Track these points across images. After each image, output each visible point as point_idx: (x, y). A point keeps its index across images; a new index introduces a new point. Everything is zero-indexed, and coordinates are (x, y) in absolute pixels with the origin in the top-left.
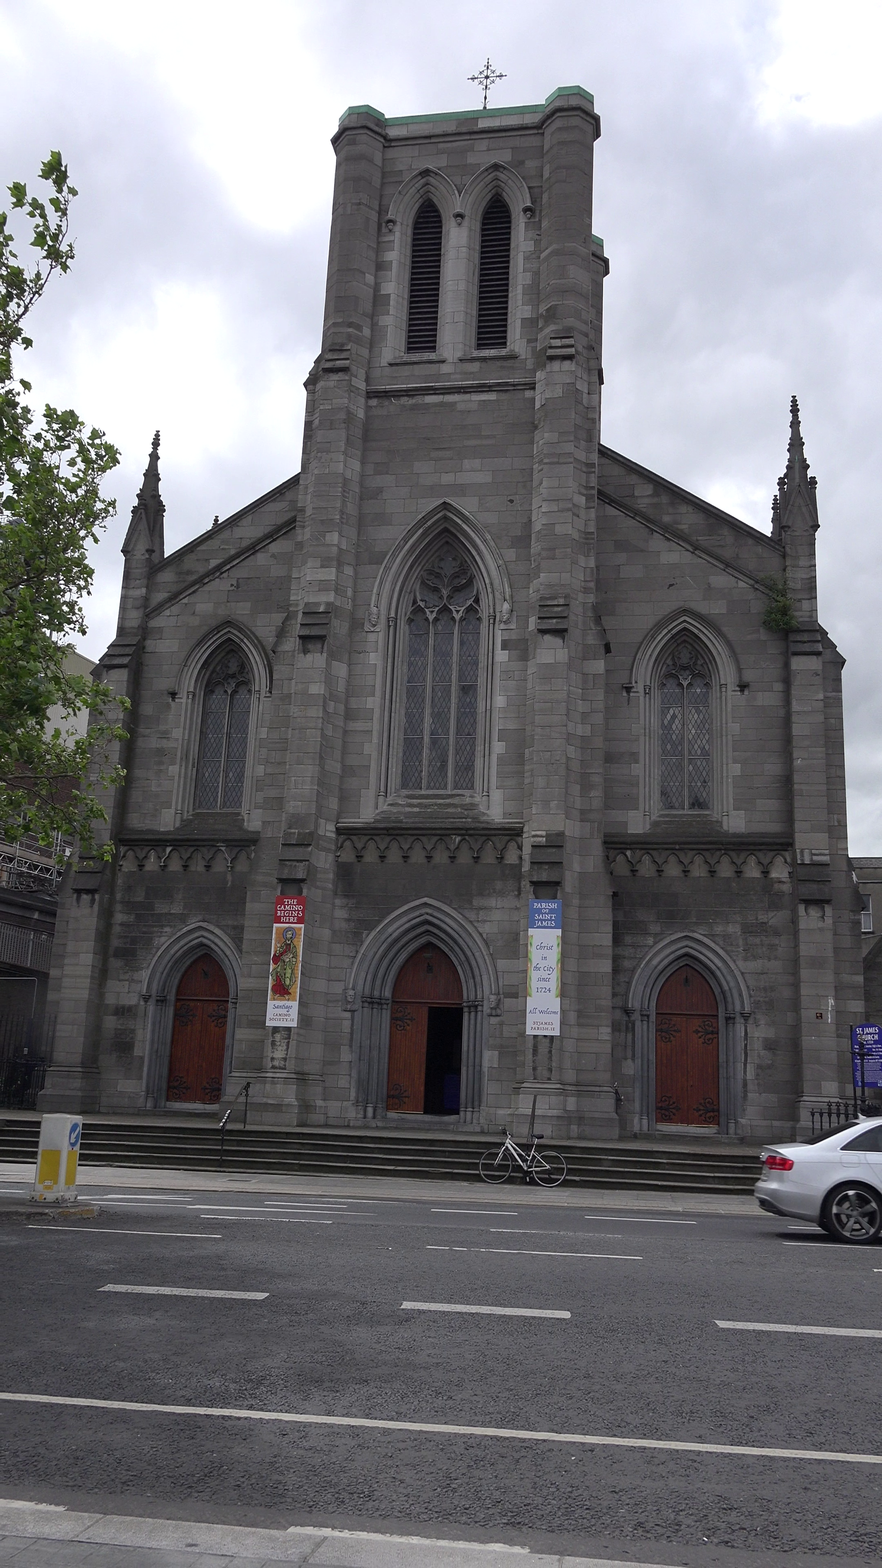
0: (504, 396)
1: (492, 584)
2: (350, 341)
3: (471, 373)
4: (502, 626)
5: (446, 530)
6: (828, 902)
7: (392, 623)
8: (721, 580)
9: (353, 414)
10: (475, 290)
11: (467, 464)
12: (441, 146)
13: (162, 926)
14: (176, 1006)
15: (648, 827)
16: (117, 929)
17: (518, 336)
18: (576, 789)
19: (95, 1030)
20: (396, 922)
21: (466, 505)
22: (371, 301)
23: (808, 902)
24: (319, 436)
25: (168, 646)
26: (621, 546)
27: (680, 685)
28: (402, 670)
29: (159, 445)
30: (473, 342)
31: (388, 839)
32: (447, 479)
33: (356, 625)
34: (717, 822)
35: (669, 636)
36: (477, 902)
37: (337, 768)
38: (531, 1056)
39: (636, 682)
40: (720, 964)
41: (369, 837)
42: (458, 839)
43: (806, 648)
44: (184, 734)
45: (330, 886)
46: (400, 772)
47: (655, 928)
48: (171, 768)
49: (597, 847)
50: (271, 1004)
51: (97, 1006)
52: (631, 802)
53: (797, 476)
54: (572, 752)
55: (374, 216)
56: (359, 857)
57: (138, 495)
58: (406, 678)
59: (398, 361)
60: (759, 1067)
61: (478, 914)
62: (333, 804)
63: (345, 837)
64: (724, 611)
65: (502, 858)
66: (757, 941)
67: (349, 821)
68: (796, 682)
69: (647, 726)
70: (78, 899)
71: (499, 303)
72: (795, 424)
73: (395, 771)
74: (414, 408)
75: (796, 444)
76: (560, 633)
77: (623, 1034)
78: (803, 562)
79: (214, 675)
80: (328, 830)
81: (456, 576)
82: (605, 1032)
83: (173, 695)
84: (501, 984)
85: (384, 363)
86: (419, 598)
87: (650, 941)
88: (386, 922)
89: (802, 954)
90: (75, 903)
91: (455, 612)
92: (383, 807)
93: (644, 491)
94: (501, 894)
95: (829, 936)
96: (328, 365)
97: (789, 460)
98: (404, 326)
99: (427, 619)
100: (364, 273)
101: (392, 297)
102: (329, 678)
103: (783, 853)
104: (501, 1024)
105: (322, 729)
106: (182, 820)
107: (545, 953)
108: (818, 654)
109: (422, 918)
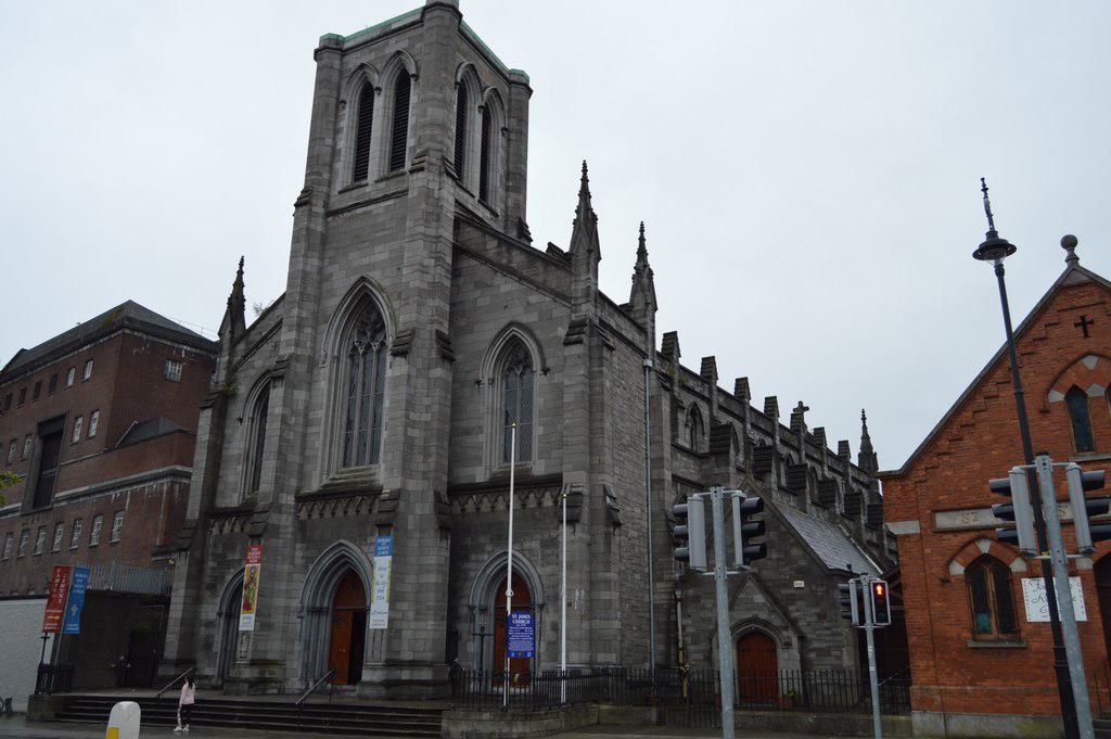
8: (535, 298)
21: (375, 275)
32: (366, 261)
33: (312, 364)
50: (242, 616)
55: (333, 101)
60: (549, 643)
66: (550, 551)
67: (305, 491)
83: (241, 420)
92: (325, 481)
107: (382, 572)
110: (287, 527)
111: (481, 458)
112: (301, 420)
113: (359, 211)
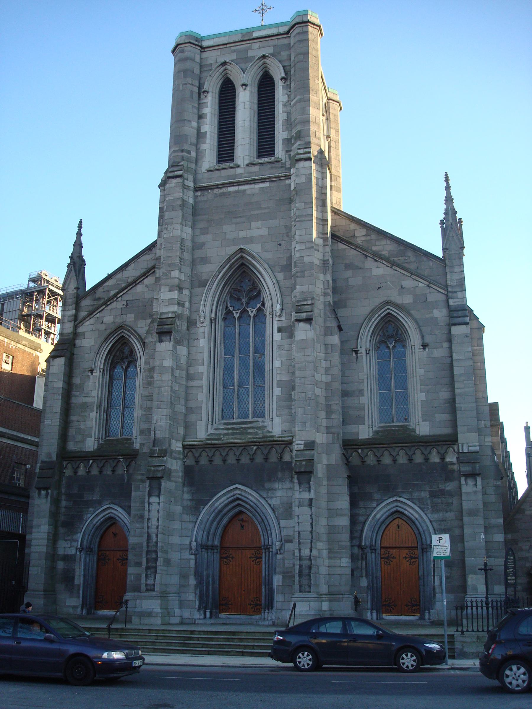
0: (273, 184)
1: (270, 294)
2: (183, 160)
3: (254, 173)
4: (277, 319)
5: (243, 264)
6: (478, 475)
7: (213, 321)
8: (408, 283)
9: (186, 201)
10: (255, 125)
11: (253, 225)
12: (233, 48)
13: (88, 508)
14: (98, 555)
15: (371, 434)
16: (63, 510)
17: (280, 149)
18: (323, 414)
19: (51, 570)
20: (220, 500)
21: (254, 249)
22: (196, 136)
23: (467, 476)
24: (167, 215)
25: (89, 341)
26: (348, 266)
27: (388, 347)
28: (220, 348)
29: (82, 227)
30: (255, 154)
31: (214, 450)
32: (242, 234)
33: (191, 323)
34: (413, 429)
35: (379, 318)
36: (267, 485)
37: (183, 409)
38: (298, 578)
39: (361, 347)
40: (417, 516)
41: (202, 449)
42: (255, 448)
43: (460, 320)
44: (98, 394)
45: (180, 480)
46: (221, 409)
47: (377, 496)
48: (91, 414)
49: (337, 450)
51: (52, 556)
52: (360, 420)
53: (450, 218)
54: (319, 392)
55: (196, 90)
56: (197, 462)
57: (70, 257)
58: (223, 353)
59: (212, 169)
61: (268, 493)
62: (181, 431)
63: (189, 450)
64: (412, 301)
65: (281, 458)
66: (439, 500)
68: (455, 341)
69: (369, 374)
70: (39, 494)
71: (230, 127)
72: (448, 188)
73: (218, 409)
74: (223, 194)
75: (449, 200)
76: (308, 320)
77: (360, 562)
78: (456, 269)
79: (115, 358)
80: (177, 446)
81: (250, 291)
82: (345, 562)
83: (92, 371)
84: (283, 534)
85: (204, 170)
86: (229, 305)
87: (375, 505)
88: (213, 500)
89: (464, 507)
90: (37, 495)
91: (250, 312)
92: (211, 431)
93: (360, 233)
94: (282, 480)
95: (480, 496)
96: (172, 174)
97: (445, 210)
98: (215, 148)
99: (234, 317)
100: (191, 121)
101: (208, 133)
102: (176, 357)
103: (453, 446)
104: (284, 559)
105: (171, 387)
106: (98, 444)
108: (467, 324)
109: (235, 497)
110: (177, 471)
111: (364, 418)
112: (184, 374)
113: (231, 189)
